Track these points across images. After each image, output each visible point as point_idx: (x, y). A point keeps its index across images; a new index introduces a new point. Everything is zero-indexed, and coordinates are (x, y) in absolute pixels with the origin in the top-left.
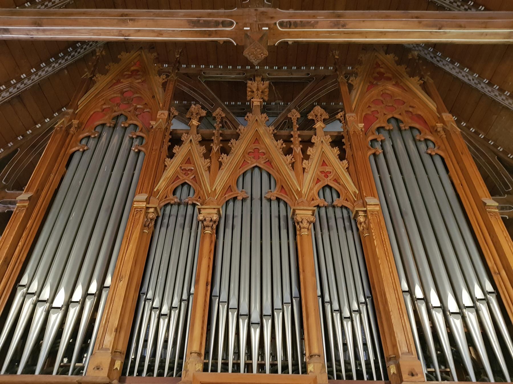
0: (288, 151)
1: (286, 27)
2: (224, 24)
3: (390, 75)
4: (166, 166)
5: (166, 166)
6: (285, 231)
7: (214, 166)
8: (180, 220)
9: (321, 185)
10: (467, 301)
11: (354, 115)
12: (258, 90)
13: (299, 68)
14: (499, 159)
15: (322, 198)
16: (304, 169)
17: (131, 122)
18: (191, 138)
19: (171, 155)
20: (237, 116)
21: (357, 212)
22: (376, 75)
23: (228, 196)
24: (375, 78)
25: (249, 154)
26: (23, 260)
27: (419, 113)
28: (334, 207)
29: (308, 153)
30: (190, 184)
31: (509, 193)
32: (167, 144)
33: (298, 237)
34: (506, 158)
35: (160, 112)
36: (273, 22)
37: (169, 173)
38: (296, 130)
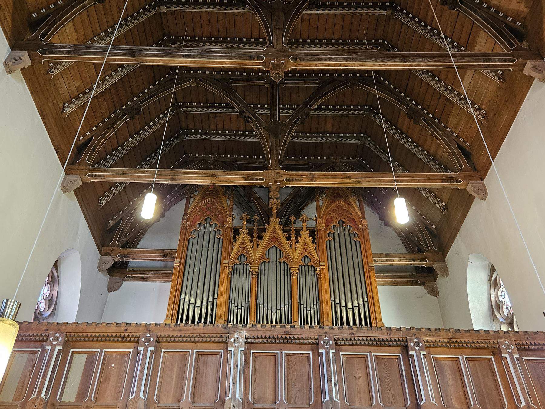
0: (289, 238)
1: (288, 181)
2: (260, 179)
3: (343, 195)
4: (233, 246)
5: (233, 246)
6: (287, 276)
7: (255, 246)
8: (242, 271)
9: (303, 255)
10: (356, 304)
11: (320, 220)
12: (275, 203)
13: (303, 158)
15: (303, 262)
16: (296, 248)
17: (214, 222)
19: (235, 241)
21: (317, 268)
22: (335, 194)
23: (262, 261)
24: (335, 197)
25: (271, 239)
28: (308, 266)
31: (427, 251)
33: (292, 279)
35: (228, 218)
37: (235, 250)
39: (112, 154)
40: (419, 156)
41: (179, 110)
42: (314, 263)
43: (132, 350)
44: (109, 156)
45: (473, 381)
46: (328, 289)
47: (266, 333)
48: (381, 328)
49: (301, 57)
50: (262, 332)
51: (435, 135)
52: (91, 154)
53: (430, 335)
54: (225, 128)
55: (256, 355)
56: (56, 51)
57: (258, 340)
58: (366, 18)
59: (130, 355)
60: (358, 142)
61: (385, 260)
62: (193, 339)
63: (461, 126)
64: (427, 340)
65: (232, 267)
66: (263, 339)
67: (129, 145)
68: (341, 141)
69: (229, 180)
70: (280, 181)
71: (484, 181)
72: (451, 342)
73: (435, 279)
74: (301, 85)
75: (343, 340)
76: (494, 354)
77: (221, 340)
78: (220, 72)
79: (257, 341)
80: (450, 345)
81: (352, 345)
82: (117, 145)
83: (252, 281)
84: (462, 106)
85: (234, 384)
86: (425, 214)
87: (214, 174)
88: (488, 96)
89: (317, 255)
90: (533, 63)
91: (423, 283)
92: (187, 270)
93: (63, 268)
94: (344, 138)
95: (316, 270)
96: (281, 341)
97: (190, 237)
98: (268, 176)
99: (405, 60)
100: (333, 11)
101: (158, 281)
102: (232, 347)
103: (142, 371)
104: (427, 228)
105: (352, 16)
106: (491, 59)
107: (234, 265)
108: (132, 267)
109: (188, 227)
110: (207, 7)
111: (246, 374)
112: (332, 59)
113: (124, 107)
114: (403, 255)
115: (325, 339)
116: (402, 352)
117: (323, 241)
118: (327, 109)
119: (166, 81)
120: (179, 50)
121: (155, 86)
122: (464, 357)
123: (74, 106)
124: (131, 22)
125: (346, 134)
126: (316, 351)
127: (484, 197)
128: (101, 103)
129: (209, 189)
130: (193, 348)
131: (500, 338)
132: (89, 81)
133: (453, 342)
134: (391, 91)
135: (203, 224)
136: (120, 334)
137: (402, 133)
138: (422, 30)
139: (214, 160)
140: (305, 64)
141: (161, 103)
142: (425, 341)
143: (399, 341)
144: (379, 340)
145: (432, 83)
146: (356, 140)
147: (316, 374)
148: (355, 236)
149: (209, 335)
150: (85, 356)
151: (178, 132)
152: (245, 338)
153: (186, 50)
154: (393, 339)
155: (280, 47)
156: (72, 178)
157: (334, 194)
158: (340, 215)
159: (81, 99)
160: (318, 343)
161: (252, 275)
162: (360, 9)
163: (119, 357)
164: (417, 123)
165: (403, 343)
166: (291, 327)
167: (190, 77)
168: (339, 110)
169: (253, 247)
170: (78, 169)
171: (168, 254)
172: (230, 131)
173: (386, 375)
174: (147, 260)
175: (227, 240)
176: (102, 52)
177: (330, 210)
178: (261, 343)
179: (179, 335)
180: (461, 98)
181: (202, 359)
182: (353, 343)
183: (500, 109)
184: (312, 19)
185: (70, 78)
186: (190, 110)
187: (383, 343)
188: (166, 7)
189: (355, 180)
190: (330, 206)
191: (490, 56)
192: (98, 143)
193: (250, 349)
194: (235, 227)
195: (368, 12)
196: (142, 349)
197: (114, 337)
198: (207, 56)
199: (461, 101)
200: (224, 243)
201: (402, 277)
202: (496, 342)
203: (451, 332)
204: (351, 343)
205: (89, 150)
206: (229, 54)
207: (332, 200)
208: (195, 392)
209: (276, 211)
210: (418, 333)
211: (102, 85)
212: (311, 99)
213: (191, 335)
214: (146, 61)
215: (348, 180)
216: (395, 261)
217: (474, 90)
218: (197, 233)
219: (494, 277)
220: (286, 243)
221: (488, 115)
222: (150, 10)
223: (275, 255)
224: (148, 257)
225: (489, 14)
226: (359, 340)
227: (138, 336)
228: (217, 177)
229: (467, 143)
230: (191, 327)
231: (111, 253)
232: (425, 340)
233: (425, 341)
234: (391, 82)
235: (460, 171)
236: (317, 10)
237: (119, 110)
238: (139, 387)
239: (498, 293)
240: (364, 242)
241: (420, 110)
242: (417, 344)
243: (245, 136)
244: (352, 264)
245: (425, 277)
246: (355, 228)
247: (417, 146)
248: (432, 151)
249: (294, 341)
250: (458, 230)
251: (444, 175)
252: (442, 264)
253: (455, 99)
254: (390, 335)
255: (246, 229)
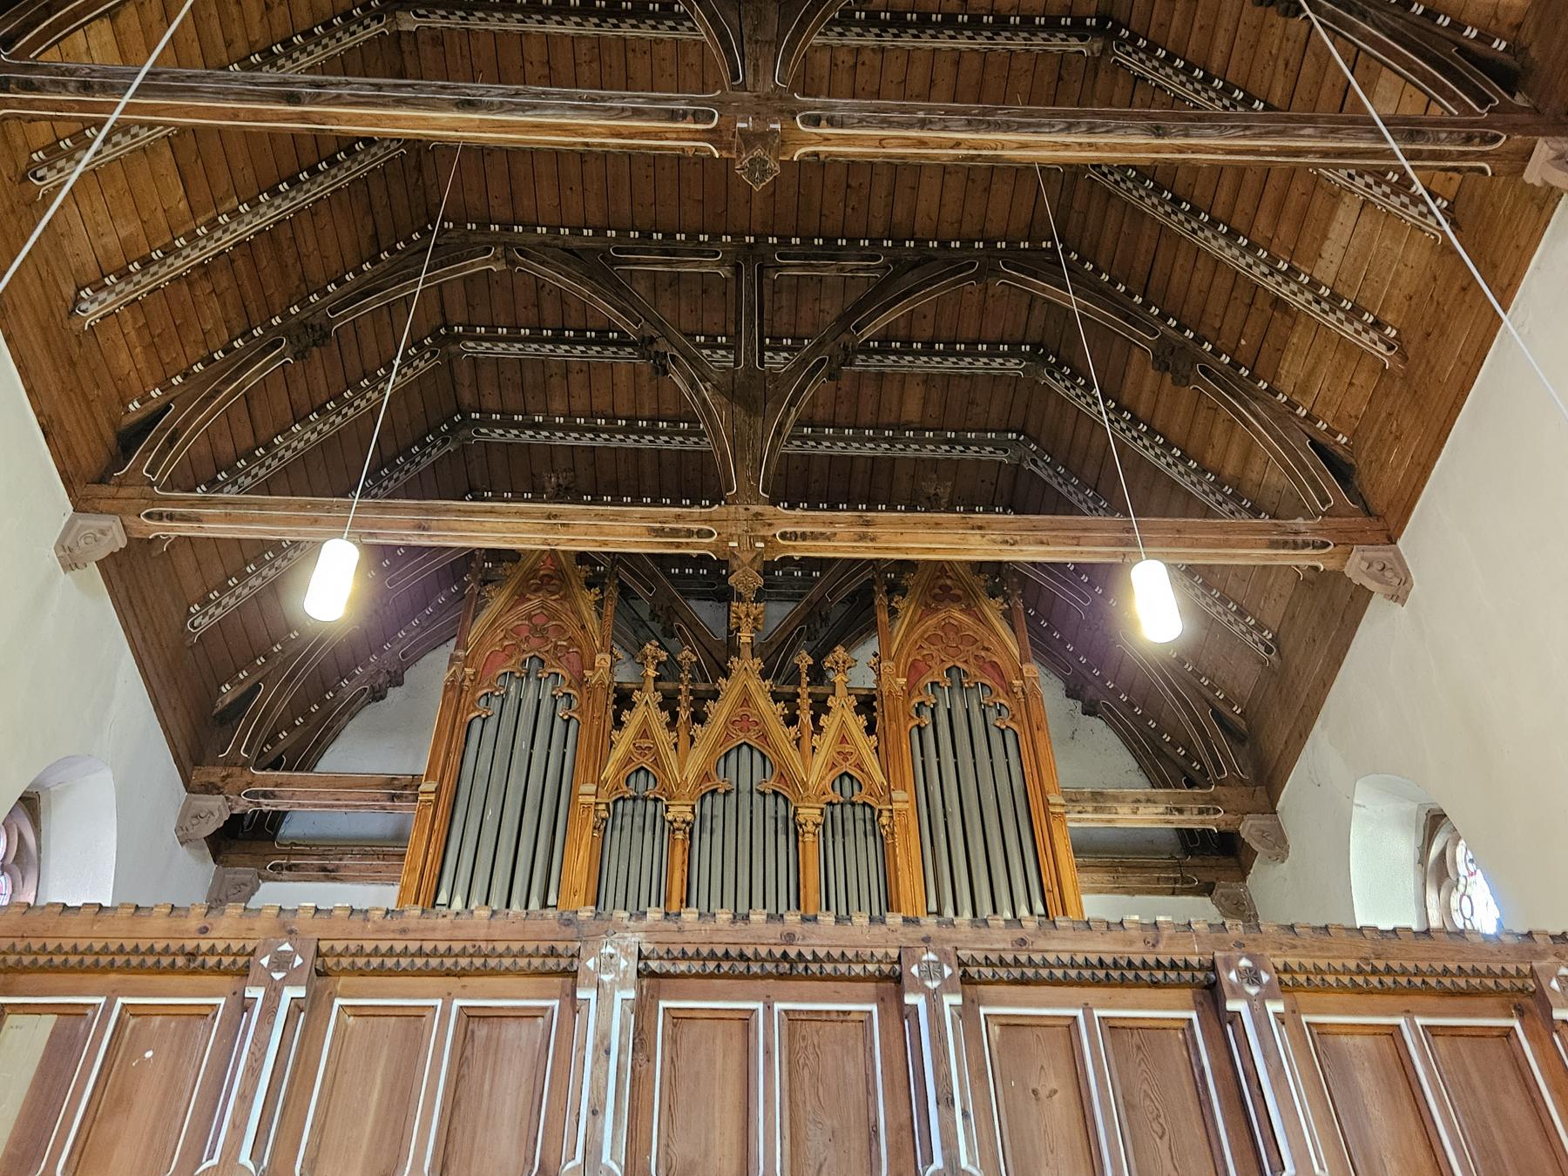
0: (791, 720)
1: (790, 540)
2: (700, 533)
3: (960, 592)
4: (612, 742)
5: (612, 742)
6: (784, 837)
7: (683, 743)
8: (638, 820)
11: (891, 664)
12: (748, 615)
14: (1217, 715)
15: (838, 792)
16: (814, 748)
17: (552, 670)
18: (647, 697)
19: (619, 724)
20: (699, 599)
21: (880, 811)
23: (705, 788)
25: (733, 723)
26: (437, 872)
27: (995, 659)
28: (853, 804)
29: (821, 723)
30: (650, 769)
31: (1220, 783)
32: (612, 708)
33: (801, 845)
34: (1230, 715)
35: (598, 657)
36: (771, 533)
37: (618, 753)
38: (805, 686)
39: (235, 468)
40: (1190, 488)
41: (453, 348)
42: (871, 795)
43: (221, 1001)
44: (223, 473)
45: (1455, 1104)
46: (918, 870)
47: (715, 940)
48: (1121, 923)
49: (833, 117)
50: (702, 937)
51: (1239, 415)
52: (162, 453)
53: (1295, 947)
54: (594, 408)
55: (677, 1019)
56: (43, 82)
57: (687, 963)
58: (1026, 67)
59: (214, 1017)
60: (1001, 456)
61: (1090, 809)
62: (449, 962)
63: (1321, 383)
64: (1285, 964)
65: (607, 805)
66: (704, 959)
67: (290, 445)
68: (950, 451)
69: (601, 534)
70: (764, 539)
71: (1400, 543)
72: (1368, 969)
73: (1243, 872)
74: (829, 272)
75: (988, 963)
76: (1521, 1013)
77: (551, 963)
78: (581, 229)
79: (683, 966)
80: (1367, 982)
81: (1023, 981)
82: (250, 442)
83: (673, 850)
84: (1324, 319)
85: (594, 1113)
86: (1208, 672)
87: (555, 517)
88: (1401, 282)
89: (882, 770)
90: (1555, 146)
91: (1208, 884)
92: (459, 817)
93: (57, 820)
94: (959, 444)
95: (879, 816)
96: (770, 967)
97: (473, 715)
98: (725, 523)
99: (1158, 132)
100: (925, 38)
101: (374, 881)
102: (590, 986)
103: (254, 1072)
104: (1217, 715)
105: (984, 55)
106: (1424, 133)
107: (615, 802)
108: (291, 838)
109: (467, 683)
110: (541, 18)
111: (639, 1082)
112: (931, 122)
113: (276, 321)
114: (1145, 794)
115: (925, 958)
116: (1198, 1006)
117: (900, 727)
118: (906, 350)
119: (411, 251)
120: (443, 87)
121: (379, 265)
122: (1420, 1021)
123: (112, 297)
124: (303, 50)
125: (963, 430)
126: (895, 1004)
127: (1400, 593)
128: (202, 299)
129: (539, 570)
130: (449, 994)
131: (1540, 955)
132: (164, 225)
133: (1375, 971)
134: (1101, 291)
135: (518, 675)
136: (181, 943)
137: (1135, 421)
138: (1198, 92)
139: (559, 485)
140: (848, 140)
141: (395, 320)
142: (1280, 967)
143: (1188, 966)
144: (1116, 965)
145: (1228, 253)
146: (995, 449)
147: (892, 1081)
148: (1000, 715)
149: (508, 948)
150: (49, 1021)
151: (448, 419)
152: (639, 958)
153: (466, 88)
154: (1165, 961)
155: (766, 87)
156: (93, 522)
157: (934, 588)
158: (951, 651)
159: (136, 279)
160: (901, 974)
161: (674, 832)
162: (1008, 34)
163: (173, 1024)
164: (1184, 381)
165: (1200, 976)
166: (804, 919)
167: (490, 243)
168: (943, 355)
169: (676, 745)
170: (118, 496)
171: (405, 787)
172: (612, 419)
173: (1145, 1086)
174: (337, 806)
175: (592, 722)
176: (192, 89)
177: (922, 637)
178: (698, 976)
179: (399, 946)
180: (1318, 295)
181: (482, 1031)
182: (1023, 973)
183: (1443, 316)
184: (863, 64)
185: (99, 205)
186: (487, 348)
187: (1130, 975)
188: (416, 14)
189: (999, 538)
190: (919, 625)
191: (1420, 124)
192: (187, 421)
193: (656, 996)
194: (620, 686)
195: (1031, 45)
196: (256, 993)
197: (159, 954)
198: (534, 107)
199: (1320, 304)
200: (584, 733)
201: (1143, 867)
202: (1526, 969)
203: (1368, 936)
204: (1016, 973)
205: (156, 439)
206: (605, 101)
207: (927, 605)
208: (450, 1146)
209: (752, 638)
210: (1254, 940)
211: (205, 240)
212: (858, 308)
213: (442, 947)
214: (337, 118)
215: (978, 537)
216: (1119, 810)
217: (1361, 269)
218: (495, 703)
219: (1435, 851)
220: (781, 735)
221: (1405, 343)
222: (366, 22)
223: (746, 771)
224: (342, 797)
225: (1406, 20)
226: (1046, 964)
227: (249, 949)
228: (562, 525)
229: (1341, 436)
230: (445, 920)
231: (220, 784)
232: (1280, 964)
233: (1280, 967)
234: (1101, 264)
235: (1324, 515)
236: (877, 35)
237: (259, 329)
238: (238, 1128)
239: (1448, 903)
240: (1028, 731)
241: (1191, 344)
242: (1252, 976)
243: (657, 433)
244: (992, 797)
245: (1212, 867)
246: (1000, 690)
247: (1184, 458)
248: (1230, 469)
249: (814, 967)
250: (1316, 711)
251: (1276, 524)
252: (1268, 822)
253: (1300, 298)
254: (1154, 946)
255: (656, 690)
